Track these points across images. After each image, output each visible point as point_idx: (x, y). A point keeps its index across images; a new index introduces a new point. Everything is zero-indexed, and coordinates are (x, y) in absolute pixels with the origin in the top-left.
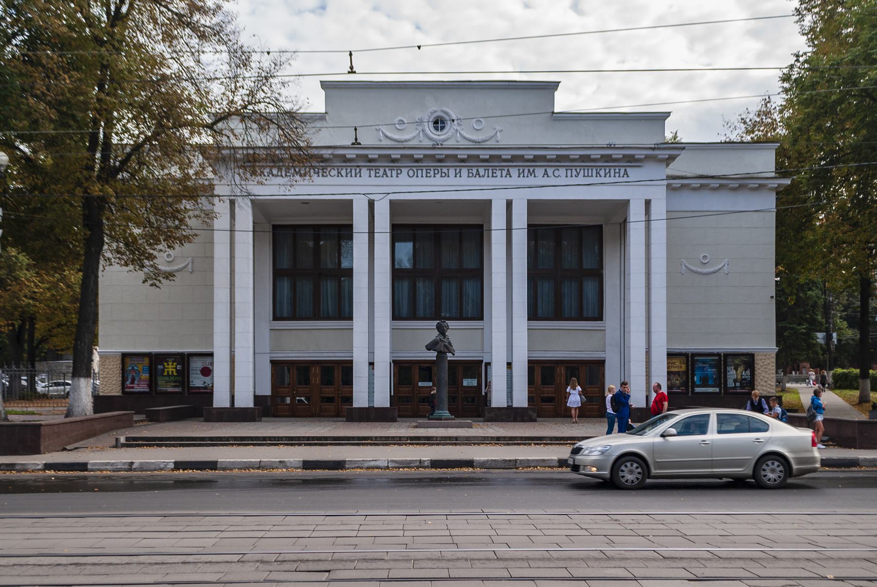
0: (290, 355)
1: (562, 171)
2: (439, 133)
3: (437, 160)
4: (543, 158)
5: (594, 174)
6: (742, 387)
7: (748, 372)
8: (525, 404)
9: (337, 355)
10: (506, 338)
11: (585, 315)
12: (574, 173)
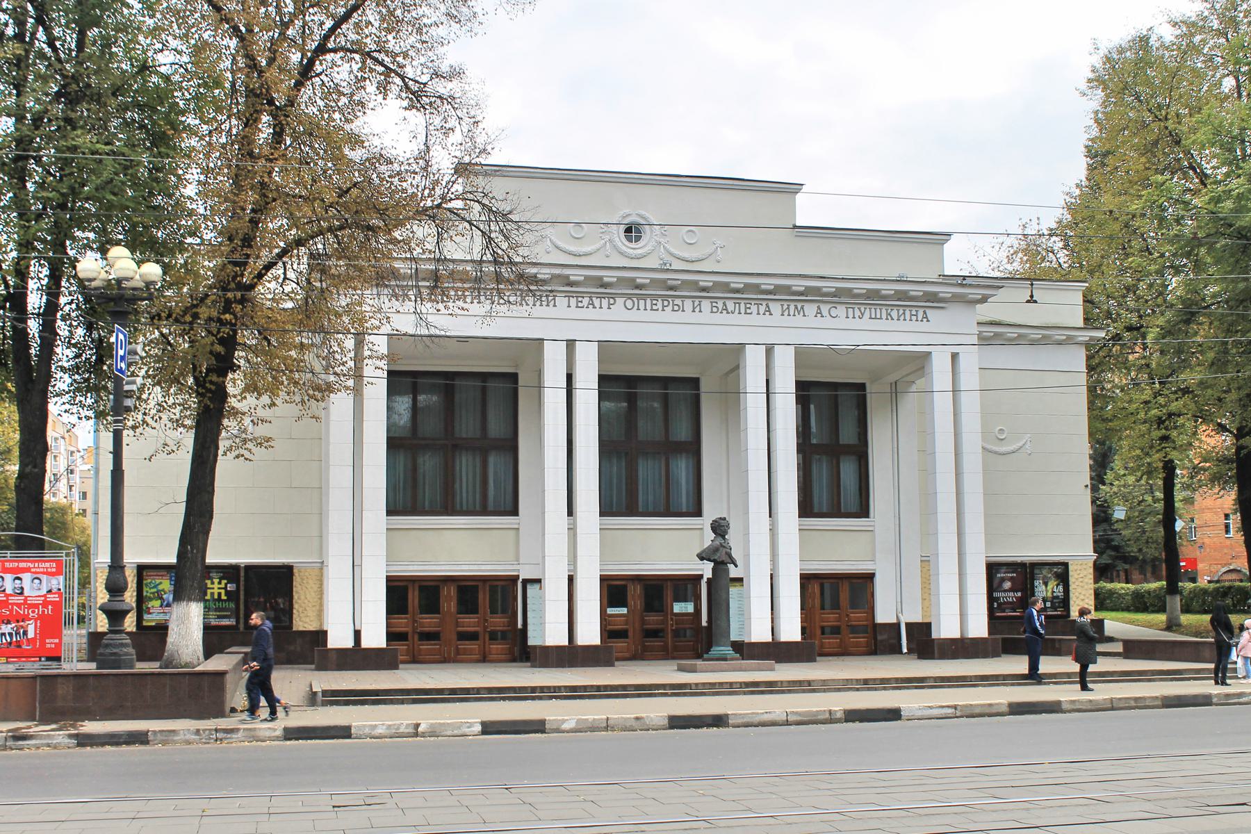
0: (411, 568)
1: (841, 310)
2: (633, 245)
3: (668, 288)
4: (817, 291)
5: (884, 316)
6: (1054, 608)
7: (1061, 588)
8: (596, 641)
9: (483, 567)
10: (563, 544)
11: (816, 510)
12: (857, 313)
